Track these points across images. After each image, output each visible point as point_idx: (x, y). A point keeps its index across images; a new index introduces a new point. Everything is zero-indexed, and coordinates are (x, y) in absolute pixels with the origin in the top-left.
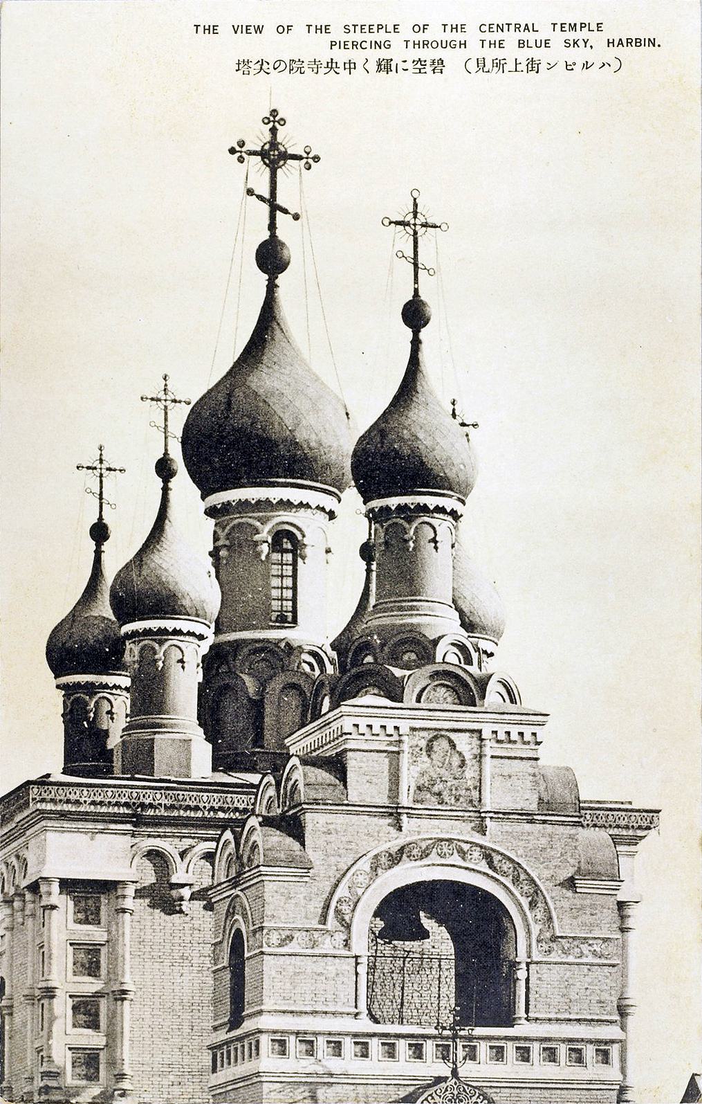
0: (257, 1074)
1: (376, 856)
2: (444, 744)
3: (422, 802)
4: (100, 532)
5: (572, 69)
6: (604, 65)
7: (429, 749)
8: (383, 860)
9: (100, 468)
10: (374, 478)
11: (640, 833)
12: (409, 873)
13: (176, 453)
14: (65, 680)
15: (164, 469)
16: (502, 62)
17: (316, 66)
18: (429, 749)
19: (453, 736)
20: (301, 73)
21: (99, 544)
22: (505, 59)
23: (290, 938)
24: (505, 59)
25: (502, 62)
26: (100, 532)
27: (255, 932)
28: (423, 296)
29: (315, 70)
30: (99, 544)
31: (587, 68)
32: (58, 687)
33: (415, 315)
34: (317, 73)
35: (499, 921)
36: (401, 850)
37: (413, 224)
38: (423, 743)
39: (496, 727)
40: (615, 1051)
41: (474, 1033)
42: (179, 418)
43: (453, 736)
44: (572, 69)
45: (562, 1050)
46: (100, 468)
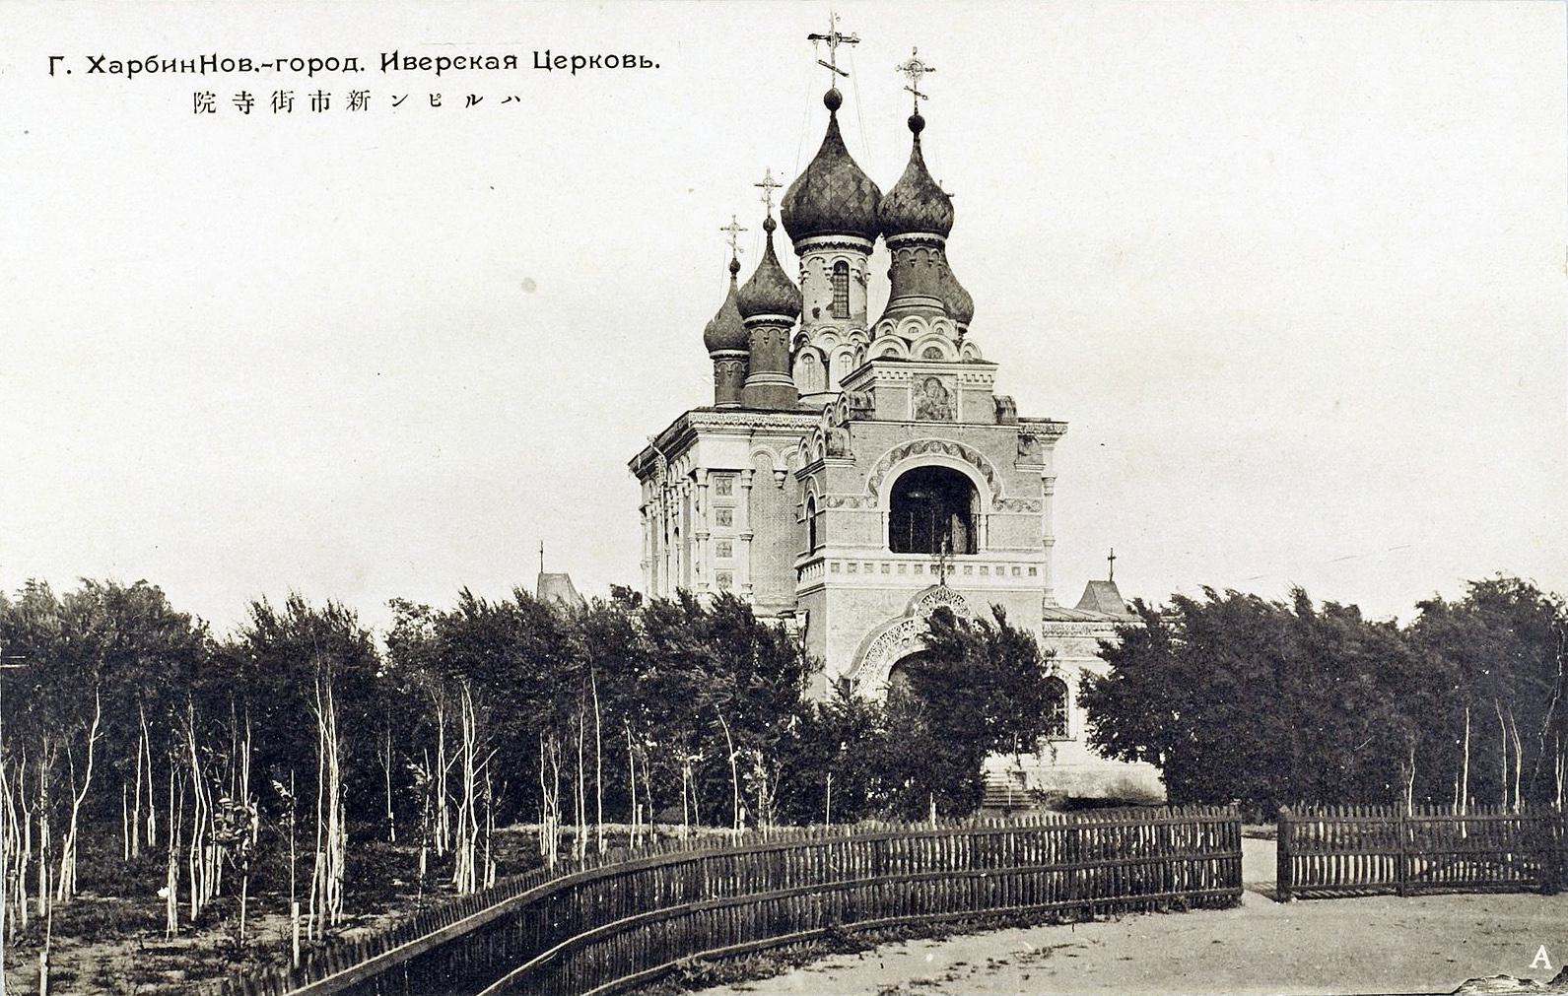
0: (822, 585)
1: (893, 452)
2: (935, 383)
3: (922, 418)
4: (735, 268)
5: (440, 104)
6: (510, 99)
7: (926, 385)
8: (899, 454)
9: (734, 229)
10: (367, 753)
11: (1055, 436)
12: (913, 462)
13: (777, 218)
14: (714, 353)
15: (769, 227)
16: (365, 95)
17: (246, 103)
18: (926, 385)
19: (940, 378)
20: (209, 111)
21: (916, 134)
22: (368, 91)
23: (842, 503)
24: (368, 91)
25: (365, 95)
26: (735, 268)
27: (821, 498)
28: (920, 113)
29: (245, 109)
30: (916, 134)
31: (474, 103)
32: (711, 357)
33: (916, 124)
34: (247, 113)
35: (969, 492)
36: (909, 448)
37: (913, 68)
38: (921, 382)
39: (965, 372)
40: (1040, 568)
41: (955, 558)
42: (777, 197)
43: (940, 378)
44: (440, 104)
45: (1008, 568)
46: (734, 229)
